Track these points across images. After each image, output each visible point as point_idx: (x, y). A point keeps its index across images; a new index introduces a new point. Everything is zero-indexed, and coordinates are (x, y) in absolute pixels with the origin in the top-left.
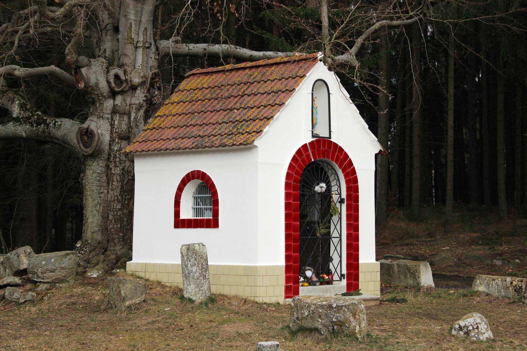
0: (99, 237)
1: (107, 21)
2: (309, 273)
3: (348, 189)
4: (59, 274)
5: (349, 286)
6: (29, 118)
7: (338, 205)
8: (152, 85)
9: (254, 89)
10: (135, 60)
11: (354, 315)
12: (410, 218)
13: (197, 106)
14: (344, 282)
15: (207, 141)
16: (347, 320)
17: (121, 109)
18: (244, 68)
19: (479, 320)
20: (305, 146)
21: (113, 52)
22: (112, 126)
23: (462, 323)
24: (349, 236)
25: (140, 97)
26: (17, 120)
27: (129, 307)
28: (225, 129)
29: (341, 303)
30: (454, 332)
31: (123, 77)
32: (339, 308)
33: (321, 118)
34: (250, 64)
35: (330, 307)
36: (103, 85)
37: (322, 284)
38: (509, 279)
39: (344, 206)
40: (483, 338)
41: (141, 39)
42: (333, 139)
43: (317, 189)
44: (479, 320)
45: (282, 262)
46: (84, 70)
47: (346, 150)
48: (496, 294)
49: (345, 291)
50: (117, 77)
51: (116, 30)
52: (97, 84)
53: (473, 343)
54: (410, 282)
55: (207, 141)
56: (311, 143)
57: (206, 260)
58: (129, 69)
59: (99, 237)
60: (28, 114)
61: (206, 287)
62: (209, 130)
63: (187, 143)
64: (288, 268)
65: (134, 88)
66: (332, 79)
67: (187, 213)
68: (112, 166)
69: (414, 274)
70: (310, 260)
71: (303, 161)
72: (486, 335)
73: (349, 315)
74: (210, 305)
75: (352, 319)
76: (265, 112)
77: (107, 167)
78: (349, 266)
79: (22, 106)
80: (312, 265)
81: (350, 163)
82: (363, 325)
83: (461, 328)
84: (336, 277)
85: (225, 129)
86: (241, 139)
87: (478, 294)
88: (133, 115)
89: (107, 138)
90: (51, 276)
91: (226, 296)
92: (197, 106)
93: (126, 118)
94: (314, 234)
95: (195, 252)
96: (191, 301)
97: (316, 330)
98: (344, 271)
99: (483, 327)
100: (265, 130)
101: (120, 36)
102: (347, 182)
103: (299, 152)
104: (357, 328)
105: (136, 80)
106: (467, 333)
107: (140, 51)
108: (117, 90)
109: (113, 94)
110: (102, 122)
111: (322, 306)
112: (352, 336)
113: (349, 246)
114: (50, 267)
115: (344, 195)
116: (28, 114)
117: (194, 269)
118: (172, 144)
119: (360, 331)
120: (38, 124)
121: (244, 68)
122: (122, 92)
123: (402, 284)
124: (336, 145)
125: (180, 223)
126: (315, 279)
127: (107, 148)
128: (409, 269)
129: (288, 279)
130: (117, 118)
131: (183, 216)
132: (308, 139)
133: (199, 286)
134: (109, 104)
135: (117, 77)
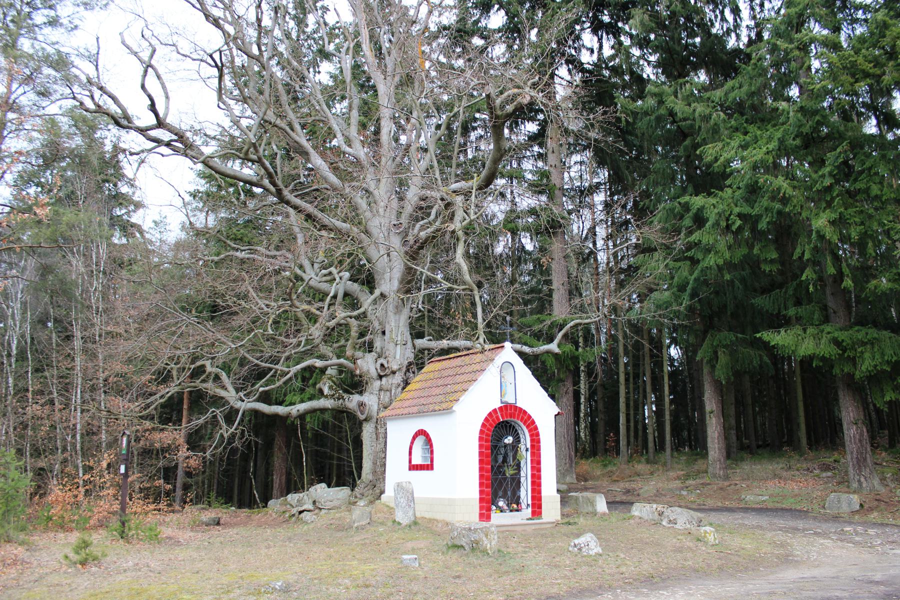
0: (370, 477)
1: (378, 328)
2: (501, 504)
3: (532, 441)
4: (336, 503)
5: (534, 513)
6: (333, 395)
7: (524, 453)
8: (408, 370)
9: (463, 370)
10: (395, 353)
11: (486, 536)
12: (648, 462)
13: (429, 384)
14: (530, 509)
15: (425, 409)
16: (481, 539)
17: (385, 387)
18: (461, 356)
19: (589, 539)
20: (495, 410)
21: (382, 349)
22: (379, 399)
23: (576, 541)
24: (533, 476)
25: (398, 378)
26: (326, 397)
27: (357, 528)
28: (441, 398)
29: (477, 526)
30: (570, 549)
31: (386, 366)
32: (475, 530)
33: (510, 389)
34: (465, 353)
35: (470, 529)
36: (374, 373)
37: (511, 511)
38: (655, 506)
39: (529, 453)
40: (592, 553)
41: (399, 339)
42: (518, 405)
43: (506, 441)
44: (589, 539)
45: (477, 496)
46: (359, 362)
47: (529, 412)
48: (646, 518)
49: (530, 516)
50: (382, 365)
51: (384, 333)
52: (368, 371)
53: (584, 556)
54: (590, 509)
55: (425, 409)
56: (500, 408)
57: (412, 493)
58: (390, 360)
59: (370, 477)
60: (333, 392)
61: (411, 513)
62: (430, 400)
63: (415, 409)
64: (481, 500)
65: (394, 373)
66: (518, 362)
67: (417, 460)
68: (379, 427)
69: (592, 503)
70: (500, 494)
71: (493, 421)
72: (595, 551)
73: (482, 535)
74: (413, 527)
75: (484, 539)
76: (464, 386)
77: (376, 427)
78: (533, 498)
79: (330, 388)
80: (504, 496)
81: (533, 422)
82: (493, 543)
83: (575, 546)
84: (524, 506)
85: (441, 398)
86: (444, 406)
87: (633, 517)
88: (393, 391)
89: (375, 408)
90: (329, 505)
91: (437, 520)
92: (429, 384)
93: (388, 393)
94: (504, 474)
95: (403, 488)
96: (399, 524)
97: (462, 546)
98: (530, 502)
99: (592, 544)
100: (461, 399)
101: (386, 338)
102: (531, 436)
103: (490, 414)
104: (489, 546)
105: (395, 367)
106: (580, 549)
107: (399, 346)
108: (382, 374)
109: (380, 377)
110: (372, 396)
111: (465, 529)
112: (485, 552)
113: (533, 483)
114: (329, 498)
115: (529, 446)
116: (333, 392)
117: (402, 500)
118: (406, 411)
119: (491, 548)
120: (339, 399)
121: (461, 356)
122: (386, 375)
123: (586, 511)
124: (521, 409)
125: (413, 467)
126: (506, 507)
127: (375, 414)
128: (589, 499)
129: (481, 508)
130: (382, 393)
131: (413, 463)
132: (497, 405)
133: (406, 513)
134: (377, 384)
135: (382, 365)
